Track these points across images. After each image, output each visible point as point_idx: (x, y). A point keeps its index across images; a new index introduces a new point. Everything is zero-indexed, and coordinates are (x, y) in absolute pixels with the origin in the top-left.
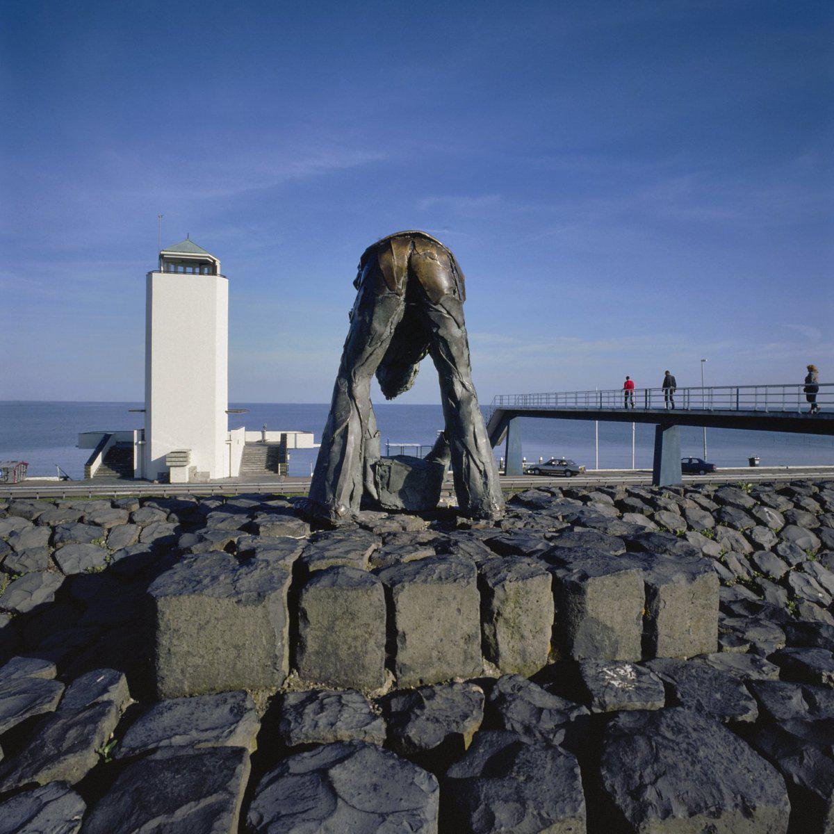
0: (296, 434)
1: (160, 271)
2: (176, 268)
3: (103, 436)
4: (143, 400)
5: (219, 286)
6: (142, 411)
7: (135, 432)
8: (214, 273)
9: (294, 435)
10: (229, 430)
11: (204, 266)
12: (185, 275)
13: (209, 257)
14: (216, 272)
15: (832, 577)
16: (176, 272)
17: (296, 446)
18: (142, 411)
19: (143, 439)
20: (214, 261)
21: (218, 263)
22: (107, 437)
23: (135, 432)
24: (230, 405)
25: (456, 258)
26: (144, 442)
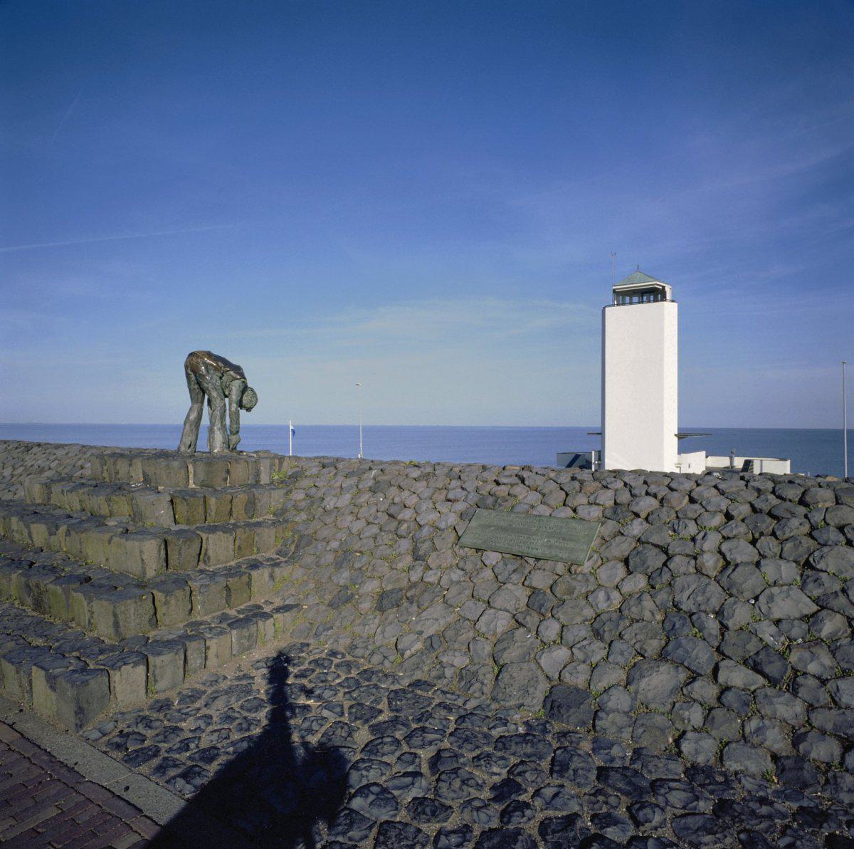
0: (761, 461)
1: (614, 305)
2: (631, 299)
3: (573, 456)
4: (600, 426)
5: (669, 311)
6: (598, 434)
7: (593, 452)
8: (664, 299)
9: (759, 462)
10: (679, 453)
11: (655, 294)
12: (624, 307)
13: (656, 284)
14: (665, 298)
15: (853, 795)
16: (631, 303)
17: (761, 470)
18: (598, 434)
19: (599, 459)
20: (664, 287)
21: (668, 289)
22: (577, 456)
23: (593, 452)
24: (678, 429)
25: (215, 352)
26: (600, 462)
